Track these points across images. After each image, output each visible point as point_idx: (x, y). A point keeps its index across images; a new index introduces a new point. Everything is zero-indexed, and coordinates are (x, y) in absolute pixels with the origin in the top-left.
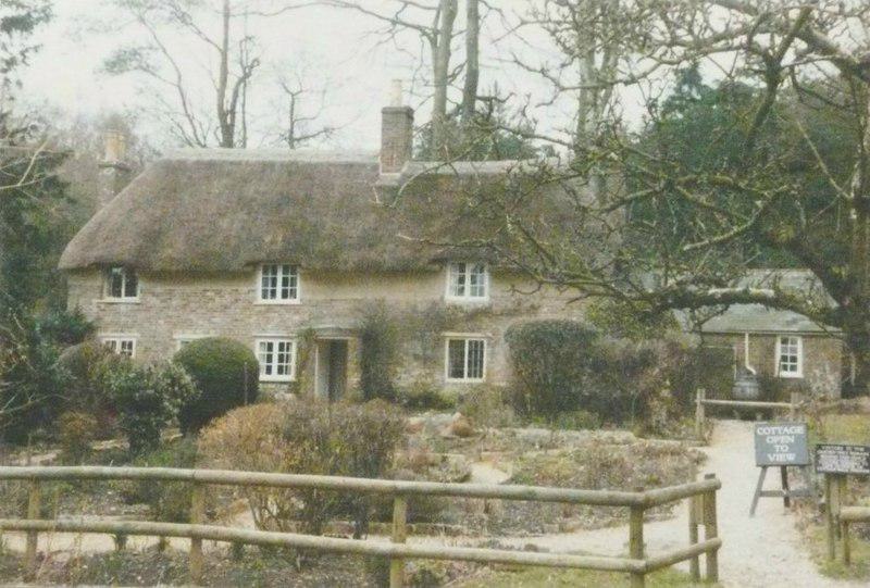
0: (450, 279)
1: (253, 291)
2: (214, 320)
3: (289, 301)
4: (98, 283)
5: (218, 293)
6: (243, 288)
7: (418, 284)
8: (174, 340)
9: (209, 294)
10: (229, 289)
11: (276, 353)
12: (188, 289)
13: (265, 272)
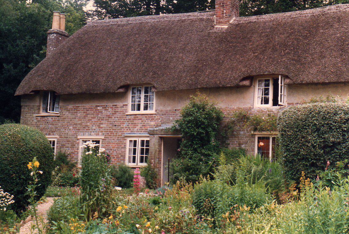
0: (257, 93)
1: (127, 105)
2: (101, 126)
3: (148, 112)
5: (105, 108)
6: (120, 104)
8: (78, 139)
9: (99, 108)
10: (110, 104)
11: (139, 147)
12: (88, 105)
13: (133, 93)
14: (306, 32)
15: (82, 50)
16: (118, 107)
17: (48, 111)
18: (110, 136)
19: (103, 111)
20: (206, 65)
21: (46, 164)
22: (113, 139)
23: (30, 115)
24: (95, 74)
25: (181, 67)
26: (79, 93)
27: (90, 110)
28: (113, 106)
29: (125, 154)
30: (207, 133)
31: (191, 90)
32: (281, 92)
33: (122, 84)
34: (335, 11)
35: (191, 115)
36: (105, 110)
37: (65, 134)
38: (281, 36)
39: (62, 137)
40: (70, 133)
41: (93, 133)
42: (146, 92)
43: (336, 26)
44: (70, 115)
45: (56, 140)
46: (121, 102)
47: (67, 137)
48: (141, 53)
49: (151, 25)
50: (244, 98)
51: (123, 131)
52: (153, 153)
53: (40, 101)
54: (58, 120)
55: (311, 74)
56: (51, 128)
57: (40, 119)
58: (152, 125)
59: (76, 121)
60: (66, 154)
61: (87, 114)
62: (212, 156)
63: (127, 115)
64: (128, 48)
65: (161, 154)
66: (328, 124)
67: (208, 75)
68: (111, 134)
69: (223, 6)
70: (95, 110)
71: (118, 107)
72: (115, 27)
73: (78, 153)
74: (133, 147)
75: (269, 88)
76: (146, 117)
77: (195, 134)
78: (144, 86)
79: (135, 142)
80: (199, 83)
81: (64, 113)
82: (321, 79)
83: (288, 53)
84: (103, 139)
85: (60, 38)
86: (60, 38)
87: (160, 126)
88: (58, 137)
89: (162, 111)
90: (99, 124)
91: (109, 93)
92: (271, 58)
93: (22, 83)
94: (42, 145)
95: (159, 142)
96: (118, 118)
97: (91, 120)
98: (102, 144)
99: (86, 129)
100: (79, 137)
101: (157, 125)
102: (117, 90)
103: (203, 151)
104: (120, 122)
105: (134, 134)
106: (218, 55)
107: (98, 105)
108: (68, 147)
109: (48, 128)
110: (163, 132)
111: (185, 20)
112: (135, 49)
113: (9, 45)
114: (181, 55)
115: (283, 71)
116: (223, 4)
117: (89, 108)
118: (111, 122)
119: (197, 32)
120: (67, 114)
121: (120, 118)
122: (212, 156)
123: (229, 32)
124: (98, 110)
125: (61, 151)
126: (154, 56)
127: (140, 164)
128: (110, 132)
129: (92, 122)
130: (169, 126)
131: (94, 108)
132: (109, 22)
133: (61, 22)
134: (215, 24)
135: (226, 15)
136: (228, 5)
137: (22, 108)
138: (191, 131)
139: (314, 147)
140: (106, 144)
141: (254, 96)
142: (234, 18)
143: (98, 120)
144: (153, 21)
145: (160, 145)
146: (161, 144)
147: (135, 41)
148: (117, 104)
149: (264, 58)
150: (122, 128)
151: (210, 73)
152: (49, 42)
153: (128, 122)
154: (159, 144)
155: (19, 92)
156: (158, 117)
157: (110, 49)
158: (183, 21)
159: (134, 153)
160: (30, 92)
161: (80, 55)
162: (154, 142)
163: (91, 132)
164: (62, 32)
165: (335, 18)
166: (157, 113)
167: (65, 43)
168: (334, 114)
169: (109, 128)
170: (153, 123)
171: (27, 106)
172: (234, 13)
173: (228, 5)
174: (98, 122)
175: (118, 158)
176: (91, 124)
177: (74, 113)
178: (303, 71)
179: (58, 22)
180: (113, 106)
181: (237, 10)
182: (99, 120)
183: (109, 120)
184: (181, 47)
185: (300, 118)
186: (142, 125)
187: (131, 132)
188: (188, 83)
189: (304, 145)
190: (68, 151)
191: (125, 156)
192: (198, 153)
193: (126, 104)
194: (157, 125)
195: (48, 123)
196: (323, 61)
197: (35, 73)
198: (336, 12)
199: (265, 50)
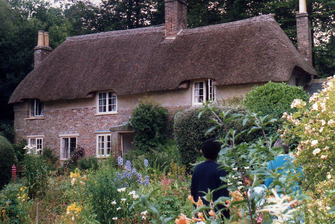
0: (194, 92)
1: (95, 108)
2: (77, 125)
3: (112, 112)
4: (26, 110)
5: (79, 110)
6: (90, 107)
7: (177, 96)
8: (59, 137)
9: (74, 111)
10: (83, 107)
11: (106, 142)
12: (65, 109)
13: (100, 97)
14: (234, 41)
15: (61, 63)
16: (89, 110)
17: (35, 115)
18: (83, 133)
19: (78, 113)
20: (154, 72)
21: (7, 161)
22: (86, 136)
23: (22, 119)
24: (70, 83)
25: (135, 74)
26: (57, 100)
27: (68, 113)
28: (85, 109)
29: (96, 148)
30: (153, 129)
31: (141, 94)
32: (211, 92)
33: (90, 91)
34: (259, 21)
35: (139, 115)
36: (79, 112)
37: (49, 133)
38: (214, 45)
39: (47, 136)
40: (53, 133)
41: (70, 132)
42: (110, 96)
43: (257, 34)
44: (52, 118)
45: (42, 139)
46: (91, 105)
47: (51, 136)
48: (106, 63)
49: (116, 39)
50: (184, 98)
51: (94, 129)
52: (114, 146)
53: (29, 108)
54: (43, 123)
55: (233, 77)
56: (38, 129)
57: (30, 122)
58: (115, 123)
59: (57, 122)
60: (51, 150)
61: (65, 116)
62: (157, 147)
63: (96, 116)
64: (96, 60)
65: (121, 146)
66: (204, 122)
67: (155, 81)
68: (85, 131)
69: (171, 21)
70: (72, 113)
71: (89, 110)
72: (87, 42)
73: (59, 149)
74: (101, 142)
75: (203, 89)
76: (110, 117)
77: (143, 130)
78: (108, 91)
79: (103, 137)
80: (148, 88)
81: (48, 116)
82: (240, 80)
83: (217, 60)
84: (78, 136)
85: (45, 53)
86: (45, 53)
87: (122, 123)
88: (44, 136)
89: (122, 111)
90: (75, 124)
91: (81, 98)
92: (203, 64)
93: (14, 93)
94: (3, 148)
95: (118, 137)
96: (89, 118)
97: (69, 121)
98: (78, 140)
99: (65, 128)
100: (60, 136)
101: (119, 123)
102: (87, 96)
103: (150, 143)
104: (91, 121)
105: (102, 131)
106: (165, 64)
107: (74, 108)
108: (52, 144)
109: (36, 129)
110: (120, 129)
111: (142, 34)
112: (102, 61)
113: (11, 58)
114: (136, 64)
115: (211, 75)
116: (171, 19)
117: (67, 111)
118: (84, 122)
119: (151, 44)
120: (50, 117)
121: (91, 118)
122: (157, 147)
123: (176, 42)
124: (74, 113)
125: (46, 148)
126: (115, 66)
127: (108, 156)
128: (83, 130)
129: (70, 123)
130: (125, 124)
131: (71, 111)
132: (83, 38)
133: (46, 40)
134: (166, 36)
135: (174, 29)
136: (175, 20)
137: (15, 113)
138: (140, 128)
139: (196, 140)
140: (80, 140)
141: (192, 95)
142: (181, 31)
143: (74, 121)
144: (117, 36)
145: (119, 140)
146: (121, 138)
147: (102, 54)
148: (88, 107)
149: (198, 64)
150: (93, 126)
151: (157, 78)
152: (36, 57)
153: (97, 121)
154: (118, 139)
155: (11, 101)
156: (119, 116)
157: (82, 61)
158: (140, 35)
159: (103, 147)
160: (20, 100)
161: (59, 67)
162: (115, 137)
163: (69, 131)
164: (47, 48)
165: (257, 27)
166: (119, 113)
167: (49, 57)
168: (209, 115)
169: (83, 127)
170: (116, 121)
171: (18, 112)
172: (181, 26)
173: (175, 20)
174: (74, 122)
175: (91, 151)
176: (69, 124)
177: (55, 116)
178: (227, 75)
179: (43, 40)
180: (85, 109)
181: (184, 23)
182: (75, 121)
183: (82, 120)
184: (137, 57)
185: (185, 119)
186: (108, 124)
187: (100, 129)
188: (140, 88)
189: (189, 139)
190: (52, 147)
191: (96, 149)
192: (147, 144)
193: (95, 106)
194: (119, 123)
195: (35, 125)
196: (243, 65)
197: (23, 84)
198: (259, 23)
199: (200, 58)
